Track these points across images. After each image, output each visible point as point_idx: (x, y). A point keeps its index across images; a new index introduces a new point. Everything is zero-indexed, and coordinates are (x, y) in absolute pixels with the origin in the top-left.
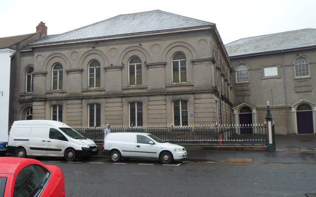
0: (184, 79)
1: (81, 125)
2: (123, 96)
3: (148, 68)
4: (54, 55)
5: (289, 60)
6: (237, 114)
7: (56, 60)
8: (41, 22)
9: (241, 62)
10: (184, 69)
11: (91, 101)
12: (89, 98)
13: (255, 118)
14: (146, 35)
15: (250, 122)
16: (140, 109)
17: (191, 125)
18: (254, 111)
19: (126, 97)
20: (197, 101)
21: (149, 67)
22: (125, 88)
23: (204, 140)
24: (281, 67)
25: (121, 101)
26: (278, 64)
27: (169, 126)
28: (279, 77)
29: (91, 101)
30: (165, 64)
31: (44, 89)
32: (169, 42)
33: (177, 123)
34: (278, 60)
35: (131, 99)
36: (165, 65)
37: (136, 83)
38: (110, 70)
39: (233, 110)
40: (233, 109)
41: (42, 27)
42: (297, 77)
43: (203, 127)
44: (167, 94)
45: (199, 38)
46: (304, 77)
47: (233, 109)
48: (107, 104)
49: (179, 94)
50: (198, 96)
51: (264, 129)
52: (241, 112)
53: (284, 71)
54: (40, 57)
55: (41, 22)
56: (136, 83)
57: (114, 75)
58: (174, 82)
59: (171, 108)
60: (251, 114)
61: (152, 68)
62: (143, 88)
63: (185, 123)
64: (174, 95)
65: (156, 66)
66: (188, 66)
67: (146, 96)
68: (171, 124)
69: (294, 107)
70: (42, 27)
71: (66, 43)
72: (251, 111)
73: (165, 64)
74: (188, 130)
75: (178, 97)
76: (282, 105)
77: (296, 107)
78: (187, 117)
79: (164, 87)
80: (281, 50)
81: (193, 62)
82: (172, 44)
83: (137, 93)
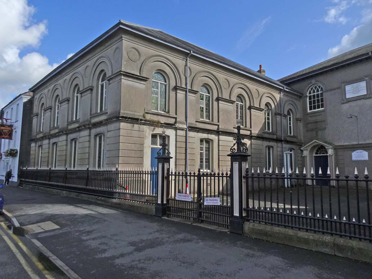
13: (331, 161)
18: (330, 152)
28: (368, 96)
39: (302, 151)
40: (302, 149)
52: (317, 153)
72: (327, 153)
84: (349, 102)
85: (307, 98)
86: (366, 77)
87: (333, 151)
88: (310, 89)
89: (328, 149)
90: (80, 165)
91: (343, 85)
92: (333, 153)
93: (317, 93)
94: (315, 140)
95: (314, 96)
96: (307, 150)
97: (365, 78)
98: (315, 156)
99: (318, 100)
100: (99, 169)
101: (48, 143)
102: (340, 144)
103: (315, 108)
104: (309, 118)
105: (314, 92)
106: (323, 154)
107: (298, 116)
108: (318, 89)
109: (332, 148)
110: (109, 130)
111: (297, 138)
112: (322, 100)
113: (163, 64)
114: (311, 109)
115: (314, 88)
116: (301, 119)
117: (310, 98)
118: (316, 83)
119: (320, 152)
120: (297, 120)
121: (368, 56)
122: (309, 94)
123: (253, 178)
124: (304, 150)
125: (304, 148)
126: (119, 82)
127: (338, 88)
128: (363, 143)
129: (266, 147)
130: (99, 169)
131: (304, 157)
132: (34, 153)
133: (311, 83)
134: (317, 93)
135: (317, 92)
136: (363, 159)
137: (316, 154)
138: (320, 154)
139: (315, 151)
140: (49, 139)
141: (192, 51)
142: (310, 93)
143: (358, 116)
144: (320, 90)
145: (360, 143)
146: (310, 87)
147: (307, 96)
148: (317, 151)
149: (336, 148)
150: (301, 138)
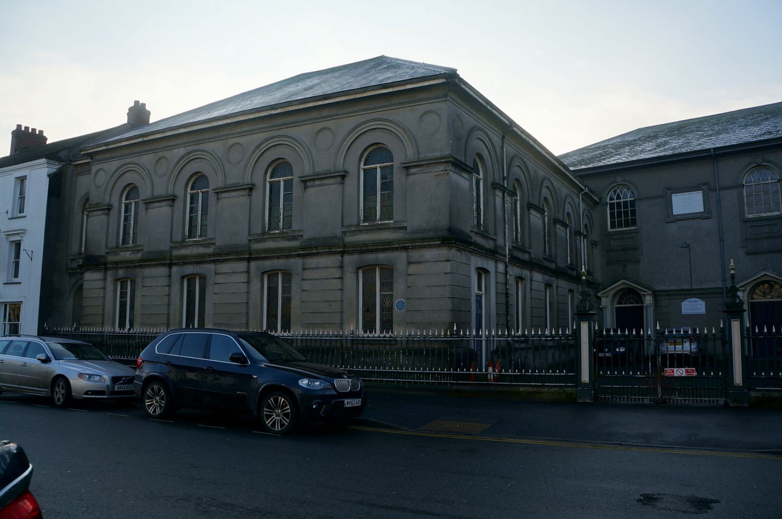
0: (388, 212)
1: (103, 324)
2: (250, 256)
3: (306, 187)
4: (124, 169)
5: (728, 170)
6: (609, 307)
7: (128, 178)
8: (137, 102)
9: (619, 179)
10: (387, 186)
11: (189, 269)
12: (184, 261)
13: (649, 315)
14: (301, 107)
15: (640, 325)
16: (287, 289)
17: (399, 332)
18: (648, 300)
19: (257, 259)
20: (413, 269)
21: (308, 184)
22: (256, 237)
23: (468, 370)
24: (708, 189)
25: (337, 275)
26: (704, 184)
27: (107, 329)
28: (706, 215)
29: (189, 269)
30: (343, 176)
31: (104, 242)
32: (350, 122)
33: (369, 325)
34: (703, 172)
35: (268, 264)
36: (343, 177)
37: (281, 224)
38: (227, 195)
39: (599, 299)
40: (599, 294)
41: (138, 114)
42: (750, 216)
43: (421, 335)
44: (345, 250)
45: (422, 108)
46: (769, 214)
47: (599, 294)
48: (218, 277)
49: (372, 251)
50: (416, 254)
51: (719, 343)
52: (619, 303)
53: (719, 201)
54: (101, 173)
55: (137, 102)
56: (281, 224)
57: (235, 202)
58: (364, 221)
59: (355, 285)
60: (642, 307)
61: (314, 186)
62: (294, 238)
63: (387, 325)
64: (361, 252)
65: (324, 182)
66: (398, 178)
67: (299, 255)
68: (354, 328)
69: (743, 291)
70: (138, 114)
71: (145, 139)
72: (642, 302)
73: (343, 176)
74: (393, 341)
75: (371, 257)
76: (712, 285)
77: (749, 288)
78: (391, 309)
79: (339, 233)
80: (708, 150)
81: (407, 168)
82: (361, 124)
83: (281, 250)
84: (678, 222)
85: (607, 206)
86: (704, 185)
87: (651, 299)
88: (612, 192)
89: (644, 296)
90: (143, 324)
91: (669, 192)
92: (652, 302)
93: (618, 201)
94: (623, 281)
95: (619, 204)
96: (607, 297)
97: (702, 186)
98: (616, 307)
99: (626, 213)
100: (120, 330)
101: (167, 274)
102: (664, 288)
103: (620, 226)
104: (612, 241)
105: (618, 197)
106: (630, 304)
107: (595, 236)
108: (618, 194)
109: (651, 295)
110: (412, 261)
111: (593, 276)
112: (633, 213)
113: (481, 143)
114: (613, 226)
115: (618, 191)
116: (598, 243)
117: (612, 208)
118: (623, 183)
119: (625, 301)
120: (592, 244)
121: (709, 154)
122: (610, 200)
123: (714, 340)
124: (604, 296)
125: (602, 294)
126: (440, 174)
127: (661, 196)
128: (699, 287)
129: (183, 277)
130: (120, 330)
131: (602, 309)
132: (102, 296)
133: (617, 182)
134: (618, 201)
135: (617, 200)
136: (698, 312)
137: (618, 304)
138: (625, 304)
139: (617, 299)
140: (170, 266)
141: (587, 188)
142: (611, 199)
143: (691, 245)
144: (629, 195)
145: (694, 287)
146: (612, 188)
147: (607, 203)
148: (621, 298)
149: (655, 294)
150: (598, 277)
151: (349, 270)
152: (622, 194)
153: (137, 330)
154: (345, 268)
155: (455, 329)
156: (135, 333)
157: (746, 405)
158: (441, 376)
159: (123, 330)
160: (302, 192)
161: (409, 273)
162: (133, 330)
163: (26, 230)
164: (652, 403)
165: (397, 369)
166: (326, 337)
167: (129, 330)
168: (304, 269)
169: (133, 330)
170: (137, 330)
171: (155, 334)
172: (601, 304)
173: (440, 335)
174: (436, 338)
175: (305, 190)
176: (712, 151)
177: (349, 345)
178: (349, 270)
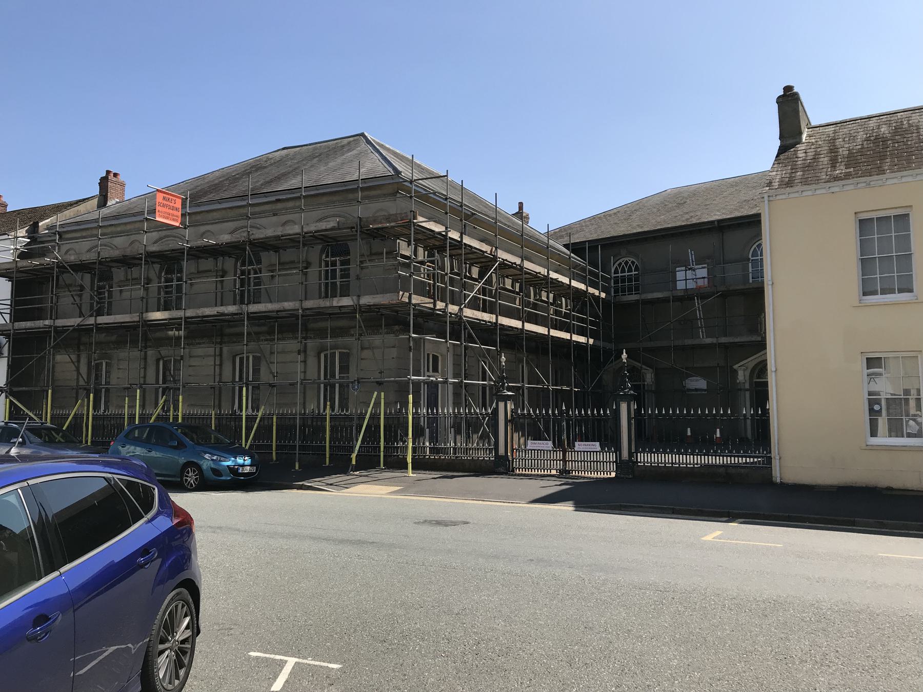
80: (712, 222)
130: (342, 411)
133: (621, 255)
151: (311, 354)
152: (626, 267)
153: (112, 412)
154: (308, 353)
155: (399, 407)
156: (110, 415)
157: (554, 472)
158: (391, 449)
159: (98, 412)
160: (270, 281)
161: (363, 357)
162: (108, 412)
163: (911, 206)
164: (558, 473)
165: (345, 444)
166: (290, 415)
167: (105, 411)
168: (363, 348)
169: (108, 412)
170: (112, 412)
171: (192, 415)
172: (738, 379)
173: (197, 413)
174: (393, 415)
175: (272, 279)
176: (716, 223)
177: (309, 422)
178: (311, 354)
